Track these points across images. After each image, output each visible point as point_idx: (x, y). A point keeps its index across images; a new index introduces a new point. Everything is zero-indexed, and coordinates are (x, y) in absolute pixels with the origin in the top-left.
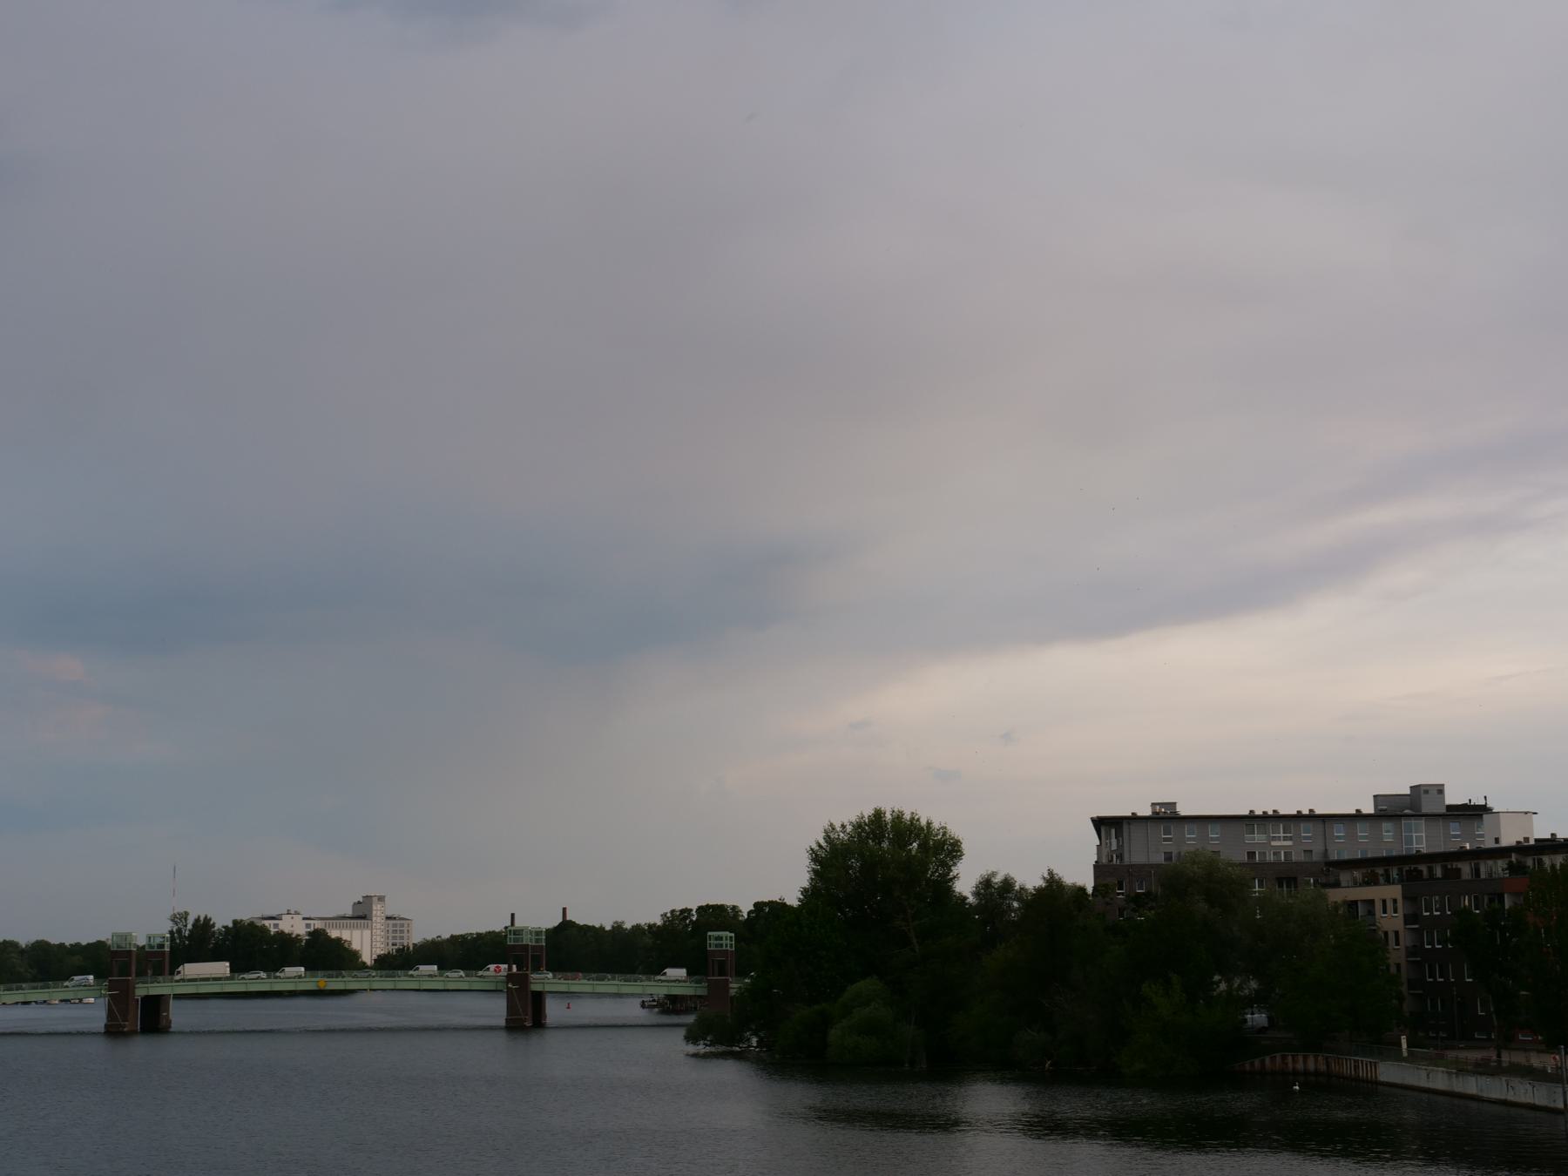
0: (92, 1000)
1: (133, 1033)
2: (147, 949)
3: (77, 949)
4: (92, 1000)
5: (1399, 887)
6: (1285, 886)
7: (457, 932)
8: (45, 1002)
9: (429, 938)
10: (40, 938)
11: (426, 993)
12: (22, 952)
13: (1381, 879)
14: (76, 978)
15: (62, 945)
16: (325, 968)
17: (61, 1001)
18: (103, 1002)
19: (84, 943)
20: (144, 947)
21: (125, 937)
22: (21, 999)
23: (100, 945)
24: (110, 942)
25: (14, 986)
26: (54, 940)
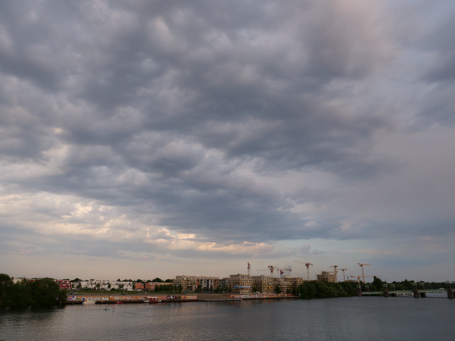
0: (444, 292)
1: (453, 298)
2: (452, 284)
3: (439, 283)
4: (444, 292)
5: (175, 279)
6: (237, 296)
7: (48, 277)
8: (436, 292)
9: (75, 279)
10: (433, 282)
11: (191, 303)
12: (430, 284)
13: (368, 291)
14: (441, 288)
15: (437, 283)
16: (399, 290)
17: (439, 292)
18: (446, 292)
19: (441, 283)
20: (452, 283)
21: (448, 282)
22: (431, 292)
23: (443, 283)
24: (445, 282)
25: (430, 289)
26: (435, 282)
